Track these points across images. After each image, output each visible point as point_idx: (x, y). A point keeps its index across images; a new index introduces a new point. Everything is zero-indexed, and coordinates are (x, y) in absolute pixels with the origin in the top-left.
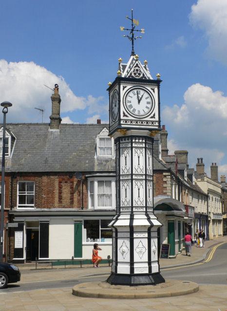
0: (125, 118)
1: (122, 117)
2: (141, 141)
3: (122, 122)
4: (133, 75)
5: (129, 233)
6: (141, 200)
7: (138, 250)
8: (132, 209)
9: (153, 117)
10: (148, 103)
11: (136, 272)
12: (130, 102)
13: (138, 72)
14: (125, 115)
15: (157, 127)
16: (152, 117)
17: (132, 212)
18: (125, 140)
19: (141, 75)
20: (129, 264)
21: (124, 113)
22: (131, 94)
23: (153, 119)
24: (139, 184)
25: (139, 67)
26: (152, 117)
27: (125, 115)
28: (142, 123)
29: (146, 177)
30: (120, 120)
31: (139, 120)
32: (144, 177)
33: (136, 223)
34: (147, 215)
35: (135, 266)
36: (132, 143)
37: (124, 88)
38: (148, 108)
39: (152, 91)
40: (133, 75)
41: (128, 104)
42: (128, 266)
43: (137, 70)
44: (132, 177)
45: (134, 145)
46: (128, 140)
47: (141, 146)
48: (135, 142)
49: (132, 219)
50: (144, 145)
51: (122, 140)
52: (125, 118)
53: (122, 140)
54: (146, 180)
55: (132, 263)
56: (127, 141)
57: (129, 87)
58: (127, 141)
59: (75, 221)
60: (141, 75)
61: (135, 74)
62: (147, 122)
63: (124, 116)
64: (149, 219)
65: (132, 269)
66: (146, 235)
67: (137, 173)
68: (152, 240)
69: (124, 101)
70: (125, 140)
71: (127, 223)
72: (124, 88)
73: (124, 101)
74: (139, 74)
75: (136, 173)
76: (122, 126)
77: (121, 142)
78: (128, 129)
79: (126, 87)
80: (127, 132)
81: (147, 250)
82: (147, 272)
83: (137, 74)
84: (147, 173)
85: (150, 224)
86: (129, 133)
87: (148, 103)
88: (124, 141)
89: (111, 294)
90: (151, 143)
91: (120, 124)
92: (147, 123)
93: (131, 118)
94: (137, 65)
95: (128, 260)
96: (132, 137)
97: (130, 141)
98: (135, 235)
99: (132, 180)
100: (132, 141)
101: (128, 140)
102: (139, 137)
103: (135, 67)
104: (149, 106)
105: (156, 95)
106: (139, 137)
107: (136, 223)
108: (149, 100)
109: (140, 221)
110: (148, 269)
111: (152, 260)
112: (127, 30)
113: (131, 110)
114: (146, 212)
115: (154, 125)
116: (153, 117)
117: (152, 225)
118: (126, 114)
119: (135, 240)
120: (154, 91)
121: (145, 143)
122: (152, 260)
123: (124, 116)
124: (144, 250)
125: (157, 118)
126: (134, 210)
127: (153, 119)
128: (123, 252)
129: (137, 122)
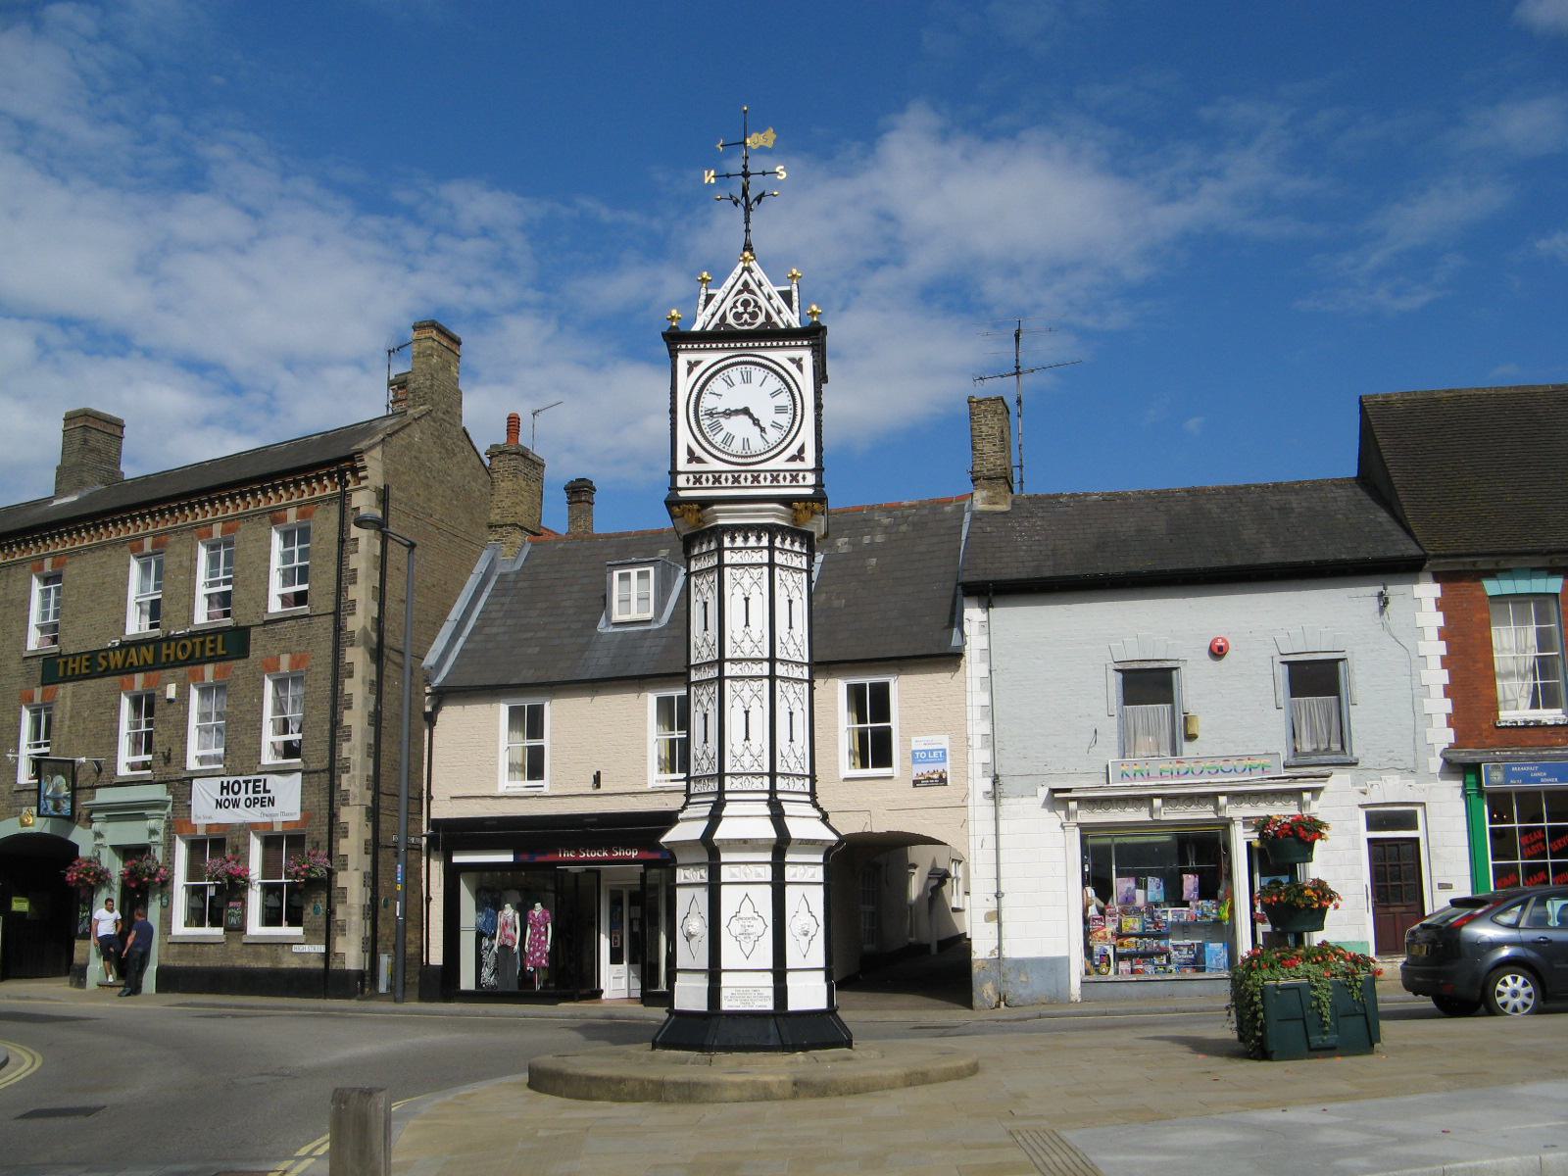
0: (695, 467)
2: (752, 542)
3: (681, 481)
4: (730, 320)
5: (769, 868)
6: (756, 750)
8: (773, 783)
9: (799, 456)
13: (750, 309)
14: (692, 457)
16: (792, 459)
17: (721, 791)
19: (761, 319)
21: (690, 452)
22: (774, 383)
25: (752, 292)
26: (792, 459)
29: (772, 669)
30: (674, 473)
31: (746, 466)
32: (765, 669)
35: (726, 979)
36: (720, 550)
37: (692, 366)
38: (781, 427)
39: (792, 368)
40: (730, 320)
42: (702, 983)
43: (746, 303)
44: (772, 669)
45: (728, 557)
48: (782, 550)
49: (715, 819)
52: (695, 467)
55: (714, 972)
58: (752, 542)
59: (1244, 818)
60: (761, 319)
61: (738, 316)
62: (775, 476)
65: (780, 992)
66: (766, 873)
67: (741, 770)
69: (798, 418)
73: (798, 418)
74: (754, 316)
75: (736, 656)
77: (778, 543)
83: (746, 316)
85: (774, 836)
88: (739, 542)
89: (71, 1105)
91: (674, 488)
92: (775, 479)
93: (715, 465)
94: (746, 284)
97: (765, 542)
98: (726, 874)
100: (721, 542)
101: (759, 539)
102: (746, 530)
103: (740, 292)
105: (806, 380)
106: (746, 530)
110: (770, 993)
112: (764, 173)
114: (773, 791)
116: (799, 456)
118: (699, 452)
119: (788, 889)
121: (771, 549)
123: (690, 461)
125: (810, 460)
127: (797, 465)
128: (689, 937)
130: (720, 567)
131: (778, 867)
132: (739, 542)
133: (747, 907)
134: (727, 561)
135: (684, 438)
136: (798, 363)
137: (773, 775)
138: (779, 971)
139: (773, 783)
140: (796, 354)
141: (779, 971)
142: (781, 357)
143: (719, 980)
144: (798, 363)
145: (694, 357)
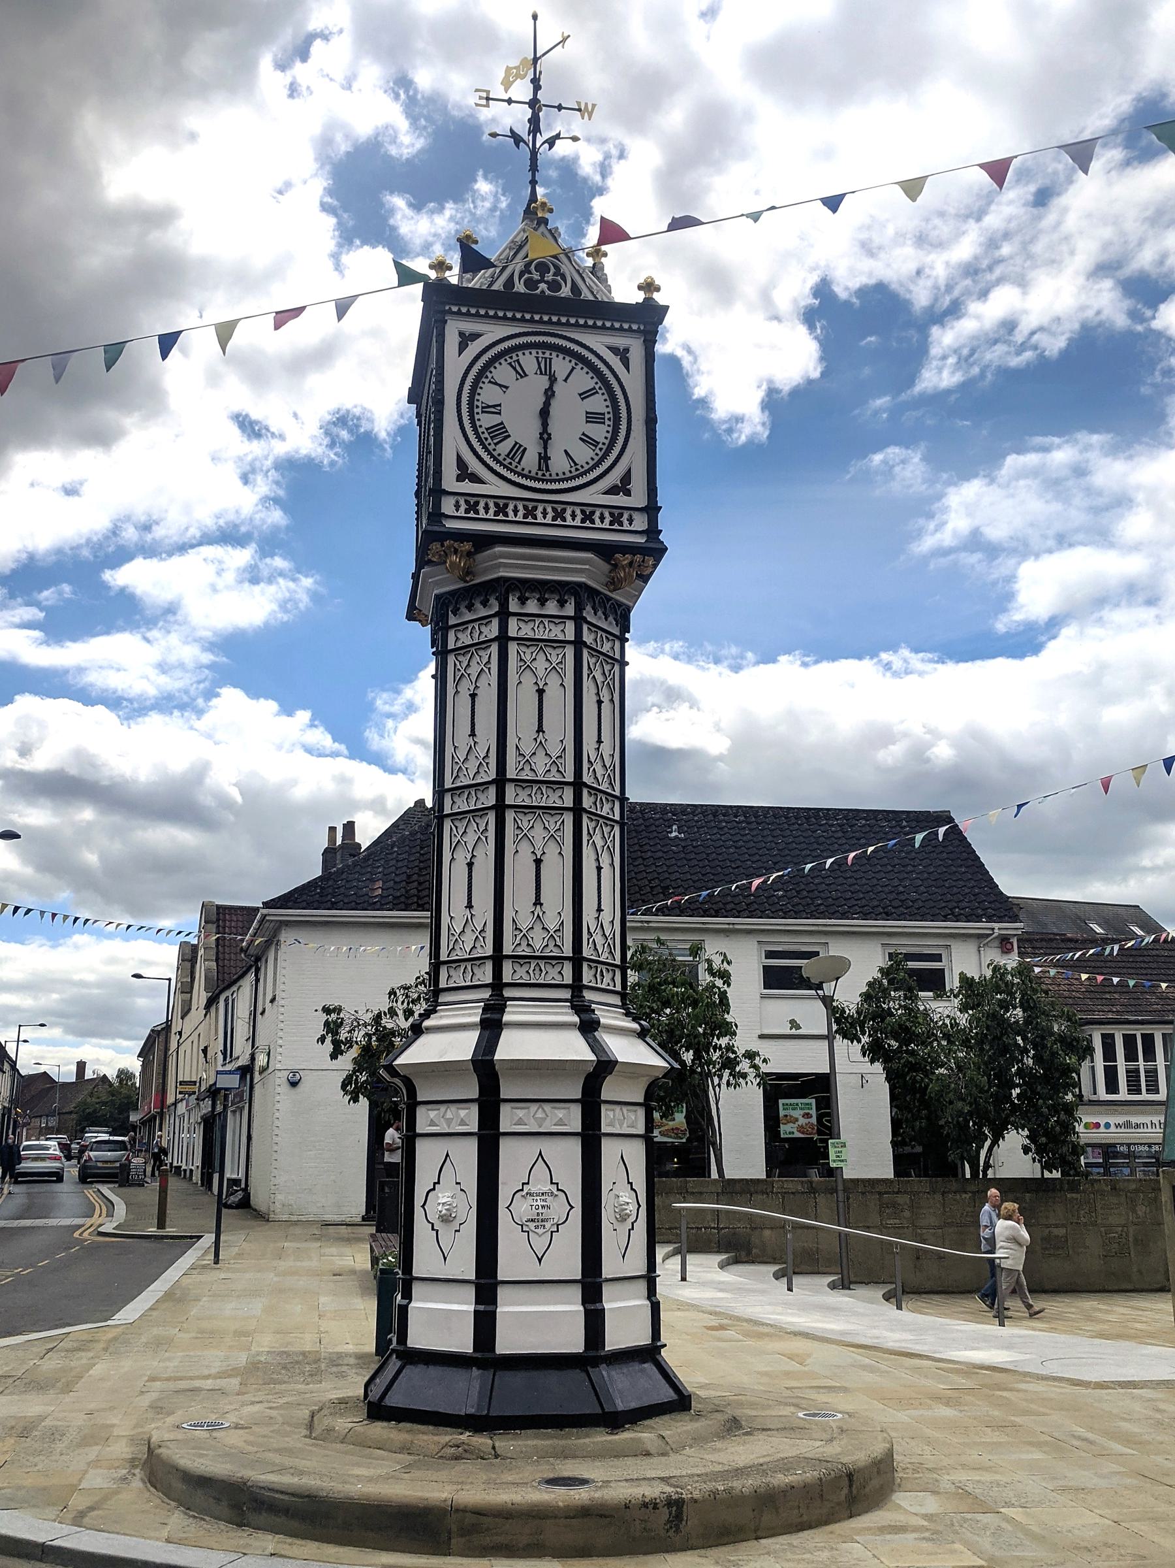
1: (449, 481)
2: (552, 608)
5: (474, 1109)
7: (523, 1209)
8: (498, 972)
9: (623, 488)
10: (593, 418)
11: (507, 1343)
12: (729, 963)
13: (549, 277)
14: (464, 473)
15: (641, 540)
16: (612, 491)
17: (497, 985)
18: (542, 602)
20: (470, 1292)
21: (461, 463)
23: (619, 500)
24: (538, 833)
26: (612, 491)
27: (464, 473)
28: (559, 515)
33: (513, 1047)
34: (581, 1008)
35: (508, 1306)
36: (504, 615)
37: (466, 340)
41: (486, 421)
42: (464, 1305)
46: (562, 603)
47: (555, 632)
49: (492, 1026)
50: (570, 627)
51: (523, 601)
52: (467, 487)
53: (523, 601)
54: (578, 811)
55: (486, 1284)
56: (483, 613)
57: (492, 332)
58: (552, 608)
63: (460, 478)
64: (589, 1027)
65: (485, 1325)
66: (573, 1119)
67: (528, 952)
68: (514, 1159)
70: (470, 607)
71: (460, 1047)
72: (466, 340)
76: (451, 524)
77: (514, 606)
78: (484, 541)
79: (475, 336)
80: (480, 557)
81: (577, 1214)
82: (462, 1341)
84: (587, 952)
85: (594, 1058)
86: (507, 564)
87: (593, 418)
88: (532, 607)
90: (616, 631)
93: (495, 487)
95: (467, 1267)
96: (503, 588)
97: (570, 610)
98: (508, 1119)
99: (500, 808)
100: (504, 604)
101: (562, 603)
102: (543, 589)
104: (600, 433)
106: (543, 589)
107: (513, 1047)
108: (599, 403)
109: (540, 1038)
111: (610, 1267)
113: (504, 448)
114: (577, 987)
115: (626, 526)
116: (623, 488)
117: (605, 1066)
118: (474, 466)
120: (626, 363)
121: (579, 620)
122: (607, 1272)
123: (460, 478)
124: (558, 1209)
125: (638, 498)
126: (507, 978)
127: (619, 500)
129: (530, 512)
130: (503, 639)
131: (489, 1105)
132: (532, 607)
133: (540, 1243)
134: (512, 632)
135: (453, 442)
136: (623, 354)
137: (577, 960)
138: (591, 1285)
139: (498, 972)
140: (620, 341)
141: (591, 1285)
142: (598, 342)
143: (494, 1301)
144: (623, 354)
145: (469, 327)
